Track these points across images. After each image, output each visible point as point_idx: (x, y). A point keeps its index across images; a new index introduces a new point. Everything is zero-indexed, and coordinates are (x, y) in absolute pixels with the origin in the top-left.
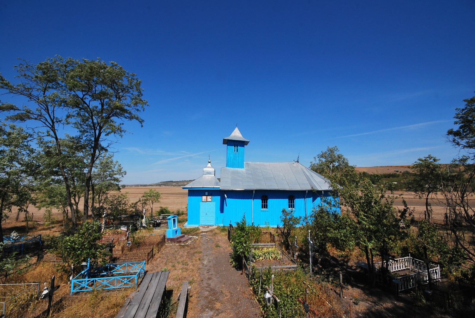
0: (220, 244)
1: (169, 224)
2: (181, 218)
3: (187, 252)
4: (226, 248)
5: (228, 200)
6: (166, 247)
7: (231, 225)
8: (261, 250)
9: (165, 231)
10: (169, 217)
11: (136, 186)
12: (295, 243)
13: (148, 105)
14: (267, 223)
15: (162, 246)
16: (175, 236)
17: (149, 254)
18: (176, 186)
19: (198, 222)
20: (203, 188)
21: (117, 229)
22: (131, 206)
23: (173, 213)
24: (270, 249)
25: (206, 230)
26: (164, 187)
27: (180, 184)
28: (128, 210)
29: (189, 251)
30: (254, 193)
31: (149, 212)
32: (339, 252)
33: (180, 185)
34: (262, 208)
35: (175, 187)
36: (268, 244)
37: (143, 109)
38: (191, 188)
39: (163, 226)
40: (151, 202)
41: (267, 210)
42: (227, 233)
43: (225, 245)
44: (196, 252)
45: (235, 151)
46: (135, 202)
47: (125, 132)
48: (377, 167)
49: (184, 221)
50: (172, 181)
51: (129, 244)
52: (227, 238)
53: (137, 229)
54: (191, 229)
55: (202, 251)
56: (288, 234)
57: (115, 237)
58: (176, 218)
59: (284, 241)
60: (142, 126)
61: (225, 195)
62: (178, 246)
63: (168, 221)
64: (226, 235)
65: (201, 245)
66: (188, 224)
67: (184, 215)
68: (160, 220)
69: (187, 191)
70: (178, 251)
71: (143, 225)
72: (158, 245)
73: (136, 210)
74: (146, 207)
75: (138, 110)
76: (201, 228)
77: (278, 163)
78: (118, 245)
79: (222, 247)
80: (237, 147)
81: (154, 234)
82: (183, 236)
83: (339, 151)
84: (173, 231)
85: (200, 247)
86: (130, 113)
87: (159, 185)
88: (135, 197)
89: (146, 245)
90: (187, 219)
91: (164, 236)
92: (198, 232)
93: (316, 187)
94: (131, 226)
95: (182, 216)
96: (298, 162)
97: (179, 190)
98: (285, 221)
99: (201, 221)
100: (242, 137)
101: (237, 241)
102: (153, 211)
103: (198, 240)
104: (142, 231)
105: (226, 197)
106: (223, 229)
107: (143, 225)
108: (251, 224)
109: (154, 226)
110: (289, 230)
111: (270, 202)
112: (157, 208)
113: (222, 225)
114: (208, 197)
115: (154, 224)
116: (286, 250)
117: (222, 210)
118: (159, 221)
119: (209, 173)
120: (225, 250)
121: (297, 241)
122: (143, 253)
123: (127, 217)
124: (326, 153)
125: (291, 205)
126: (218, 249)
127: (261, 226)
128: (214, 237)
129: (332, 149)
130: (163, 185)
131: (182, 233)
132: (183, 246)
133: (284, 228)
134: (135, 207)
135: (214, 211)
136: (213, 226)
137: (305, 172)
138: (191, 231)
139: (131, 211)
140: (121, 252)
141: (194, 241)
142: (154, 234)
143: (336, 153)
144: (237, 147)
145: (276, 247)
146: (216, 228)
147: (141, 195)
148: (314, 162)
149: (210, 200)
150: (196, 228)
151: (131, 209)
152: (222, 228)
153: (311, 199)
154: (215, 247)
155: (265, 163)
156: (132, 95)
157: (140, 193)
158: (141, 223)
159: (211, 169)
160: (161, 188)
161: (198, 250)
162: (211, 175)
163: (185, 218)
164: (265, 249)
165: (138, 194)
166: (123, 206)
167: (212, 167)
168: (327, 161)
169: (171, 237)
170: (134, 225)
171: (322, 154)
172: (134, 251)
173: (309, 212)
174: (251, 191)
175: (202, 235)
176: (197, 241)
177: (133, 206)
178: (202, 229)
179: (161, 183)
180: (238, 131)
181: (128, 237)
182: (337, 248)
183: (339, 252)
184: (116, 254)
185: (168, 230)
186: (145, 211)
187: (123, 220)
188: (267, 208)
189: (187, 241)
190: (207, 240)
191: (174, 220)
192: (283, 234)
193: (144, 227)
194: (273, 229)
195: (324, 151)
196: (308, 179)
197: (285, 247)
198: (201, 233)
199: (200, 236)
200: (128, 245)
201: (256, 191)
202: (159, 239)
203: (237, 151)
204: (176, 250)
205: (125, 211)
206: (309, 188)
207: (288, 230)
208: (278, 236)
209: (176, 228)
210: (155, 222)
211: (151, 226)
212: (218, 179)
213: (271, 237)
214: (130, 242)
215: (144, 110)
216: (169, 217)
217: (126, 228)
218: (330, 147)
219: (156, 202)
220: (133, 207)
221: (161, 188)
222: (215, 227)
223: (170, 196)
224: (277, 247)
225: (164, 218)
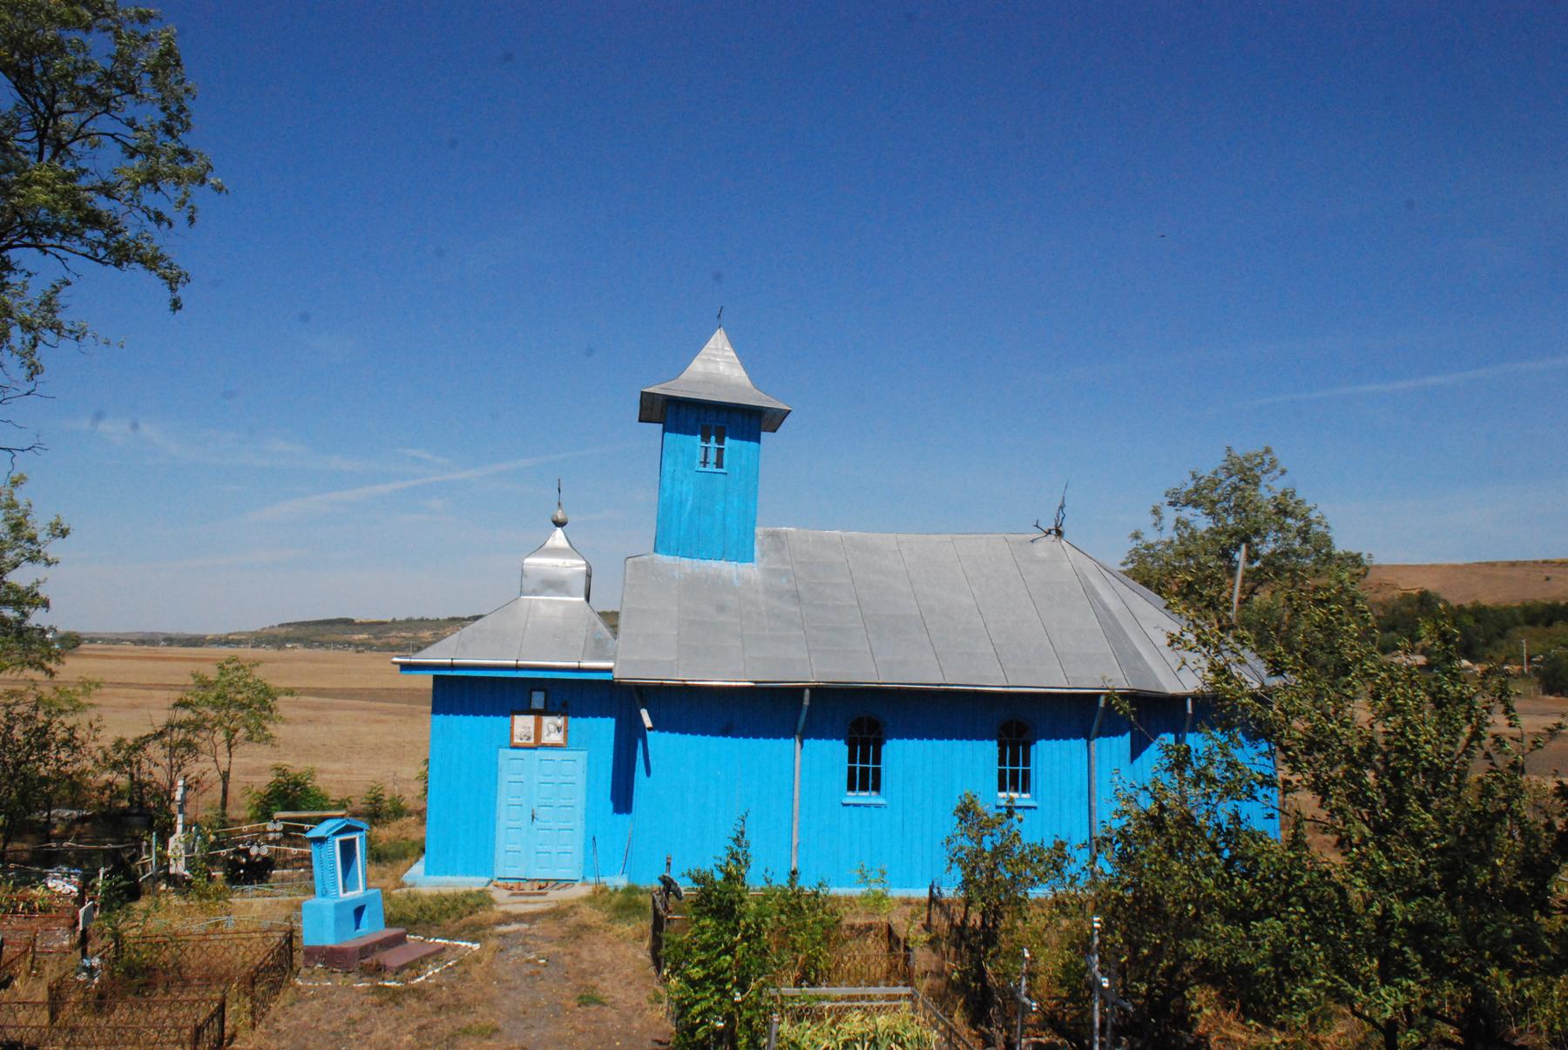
0: (607, 987)
1: (317, 870)
2: (386, 833)
3: (414, 1026)
4: (639, 1009)
5: (662, 745)
6: (300, 997)
7: (668, 884)
8: (833, 1024)
9: (298, 907)
10: (319, 831)
11: (143, 642)
12: (1018, 986)
13: (219, 189)
14: (873, 876)
15: (276, 987)
16: (354, 938)
17: (198, 1030)
18: (369, 647)
19: (483, 857)
20: (517, 668)
21: (25, 884)
22: (105, 758)
23: (342, 805)
24: (882, 1021)
25: (530, 908)
26: (300, 651)
27: (394, 637)
28: (90, 777)
29: (424, 1021)
30: (806, 702)
31: (207, 797)
32: (1258, 1030)
33: (394, 641)
34: (851, 787)
35: (368, 655)
36: (872, 990)
37: (185, 213)
38: (452, 667)
39: (283, 879)
40: (220, 736)
41: (880, 801)
42: (647, 924)
43: (632, 992)
44: (467, 1032)
45: (705, 463)
46: (131, 736)
47: (77, 338)
48: (1493, 565)
49: (404, 855)
50: (348, 622)
51: (91, 971)
52: (643, 953)
53: (134, 893)
54: (441, 899)
55: (499, 1024)
56: (990, 937)
57: (16, 930)
58: (356, 836)
59: (964, 974)
60: (176, 305)
61: (644, 713)
62: (367, 992)
63: (313, 849)
64: (642, 938)
65: (495, 990)
66: (427, 873)
67: (406, 820)
68: (268, 842)
69: (425, 681)
70: (365, 1019)
71: (172, 870)
72: (253, 983)
73: (137, 785)
74: (194, 768)
75: (159, 218)
76: (500, 895)
77: (948, 537)
78: (29, 974)
79: (614, 1005)
80: (720, 441)
81: (230, 924)
82: (399, 940)
83: (1283, 472)
84: (338, 907)
85: (490, 1001)
86: (113, 229)
87: (275, 639)
88: (134, 707)
89: (186, 983)
90: (423, 840)
91: (290, 937)
92: (481, 915)
93: (1153, 676)
94: (102, 871)
95: (395, 824)
96: (1059, 533)
97: (381, 669)
98: (970, 863)
99: (500, 856)
100: (748, 383)
101: (697, 973)
102: (234, 791)
103: (478, 960)
104: (163, 901)
105: (648, 723)
106: (626, 904)
107: (172, 870)
108: (782, 880)
109: (233, 879)
110: (993, 913)
111: (899, 754)
112: (256, 772)
113: (622, 882)
114: (546, 720)
115: (235, 865)
116: (973, 1024)
117: (622, 798)
118: (265, 851)
119: (554, 585)
120: (628, 1020)
121: (1031, 975)
122: (168, 1022)
123: (83, 819)
124: (1215, 484)
125: (1014, 777)
126: (592, 1017)
127: (835, 891)
128: (571, 948)
129: (1247, 465)
130: (298, 640)
131: (390, 922)
132: (395, 997)
133: (969, 902)
134: (130, 764)
135: (579, 798)
136: (570, 882)
137: (1096, 595)
138: (445, 913)
139: (104, 788)
140: (44, 1017)
141: (460, 969)
142: (230, 924)
143: (1268, 490)
144: (720, 441)
145: (914, 1010)
146: (589, 900)
147: (164, 694)
148: (1151, 537)
149: (557, 738)
150: (469, 895)
151: (107, 776)
152: (618, 896)
153: (1124, 742)
154: (572, 1003)
155: (876, 538)
156: (130, 132)
157: (164, 687)
158: (163, 859)
159: (569, 562)
160: (282, 660)
161: (481, 1017)
162: (569, 594)
163: (415, 835)
164: (855, 1017)
165: (149, 687)
166: (63, 756)
167: (574, 549)
168: (1220, 533)
169: (329, 940)
170: (122, 866)
171: (1191, 486)
172: (121, 1014)
173: (1108, 816)
174: (790, 695)
175: (504, 936)
176: (476, 970)
177: (119, 757)
178: (505, 902)
179: (283, 631)
180: (728, 348)
181: (84, 932)
182: (1245, 1013)
183: (1258, 1030)
184: (17, 1027)
185: (311, 902)
186: (187, 788)
187: (62, 838)
188: (877, 788)
189: (416, 965)
190: (534, 962)
191: (348, 849)
192: (962, 937)
193: (173, 880)
194: (908, 910)
195: (1206, 473)
196: (1113, 631)
197: (965, 1007)
198: (499, 923)
199: (494, 943)
200: (83, 977)
201: (818, 691)
202: (256, 952)
203: (719, 464)
204: (356, 1013)
205: (75, 786)
206: (1123, 682)
207: (983, 914)
208: (933, 943)
209: (358, 893)
210: (238, 852)
211: (218, 874)
212: (603, 615)
213: (891, 949)
214: (96, 961)
215: (191, 219)
216: (319, 831)
217: (75, 879)
218: (1239, 452)
219: (250, 739)
220: (116, 766)
221: (282, 660)
222: (580, 891)
223: (332, 707)
224: (920, 1005)
225: (292, 833)
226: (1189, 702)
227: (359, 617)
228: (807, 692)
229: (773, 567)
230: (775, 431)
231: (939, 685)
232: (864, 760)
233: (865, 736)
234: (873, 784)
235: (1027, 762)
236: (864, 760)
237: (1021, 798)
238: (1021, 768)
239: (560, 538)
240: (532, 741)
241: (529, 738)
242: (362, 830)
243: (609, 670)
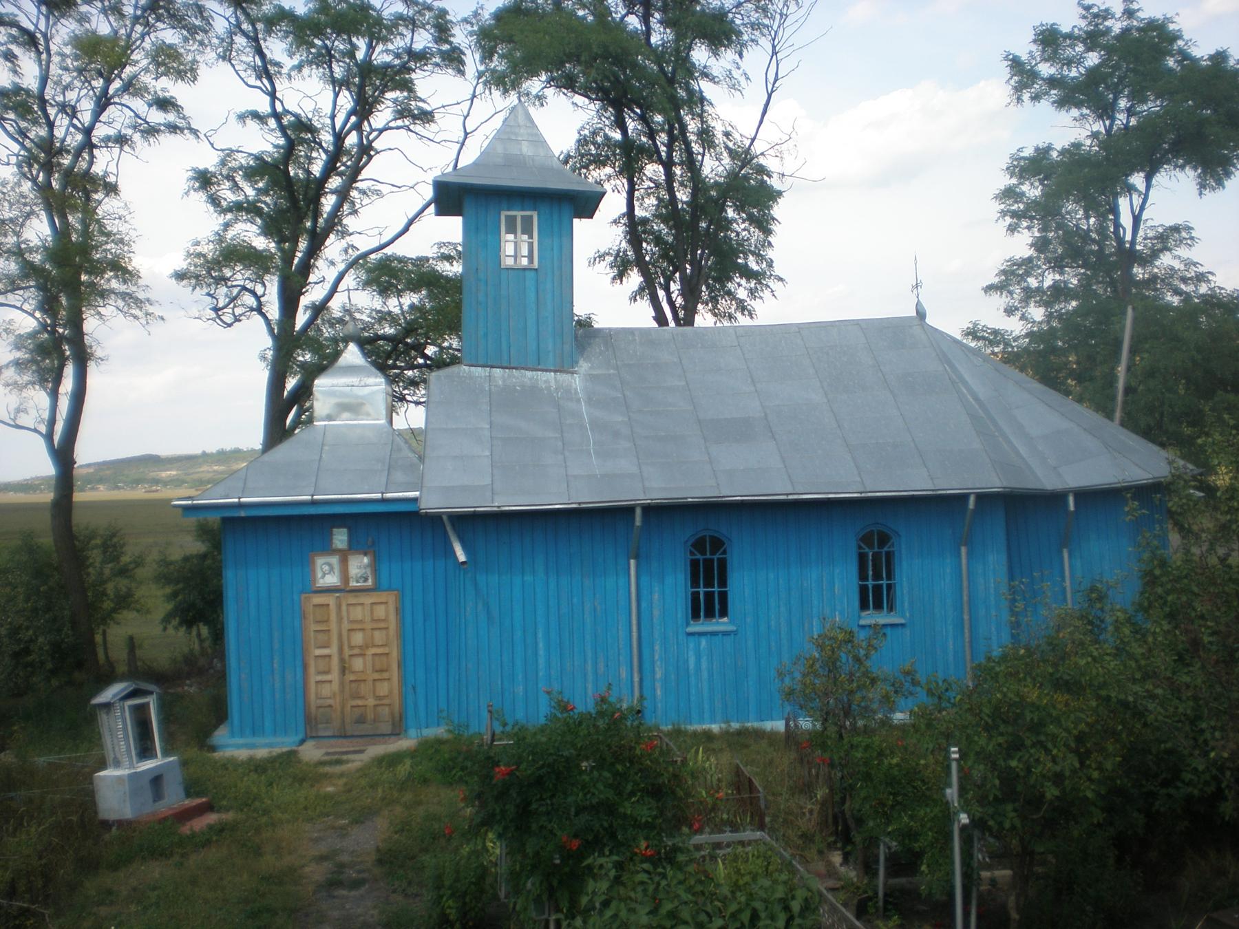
84: (134, 777)
226: (1071, 500)
227: (164, 451)
228: (638, 512)
229: (595, 373)
230: (591, 217)
231: (787, 495)
232: (709, 583)
233: (708, 556)
234: (720, 610)
235: (890, 576)
236: (709, 583)
237: (882, 618)
238: (716, 589)
239: (353, 353)
240: (370, 583)
241: (366, 580)
242: (151, 693)
243: (415, 500)
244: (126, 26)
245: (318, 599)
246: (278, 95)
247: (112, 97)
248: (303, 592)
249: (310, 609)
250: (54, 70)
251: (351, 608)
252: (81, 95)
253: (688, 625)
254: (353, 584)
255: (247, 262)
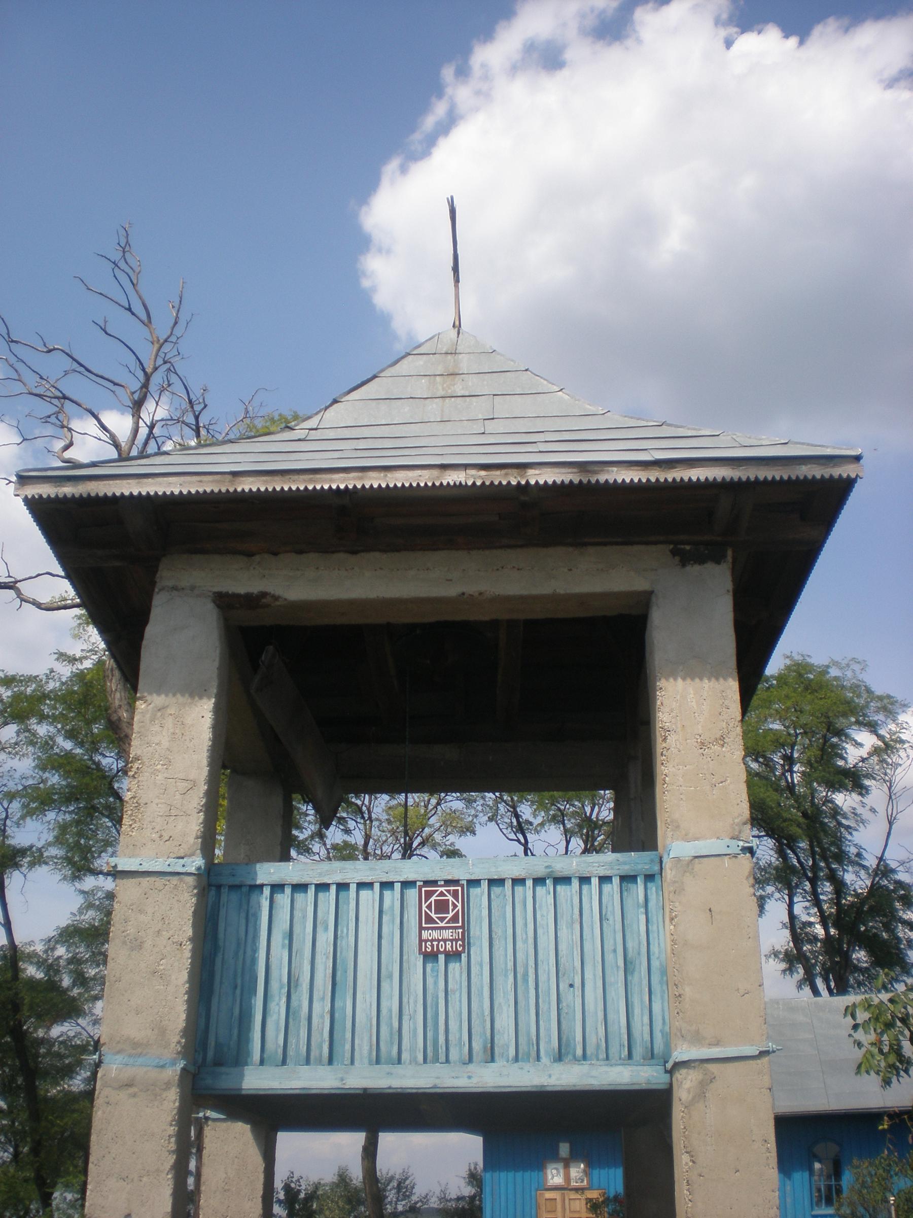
241: (582, 1181)
244: (424, 801)
245: (548, 1195)
246: (530, 845)
247: (415, 849)
248: (537, 1190)
249: (542, 1202)
250: (375, 832)
251: (572, 1202)
252: (395, 848)
253: (812, 1209)
254: (573, 1184)
255: (69, 755)
